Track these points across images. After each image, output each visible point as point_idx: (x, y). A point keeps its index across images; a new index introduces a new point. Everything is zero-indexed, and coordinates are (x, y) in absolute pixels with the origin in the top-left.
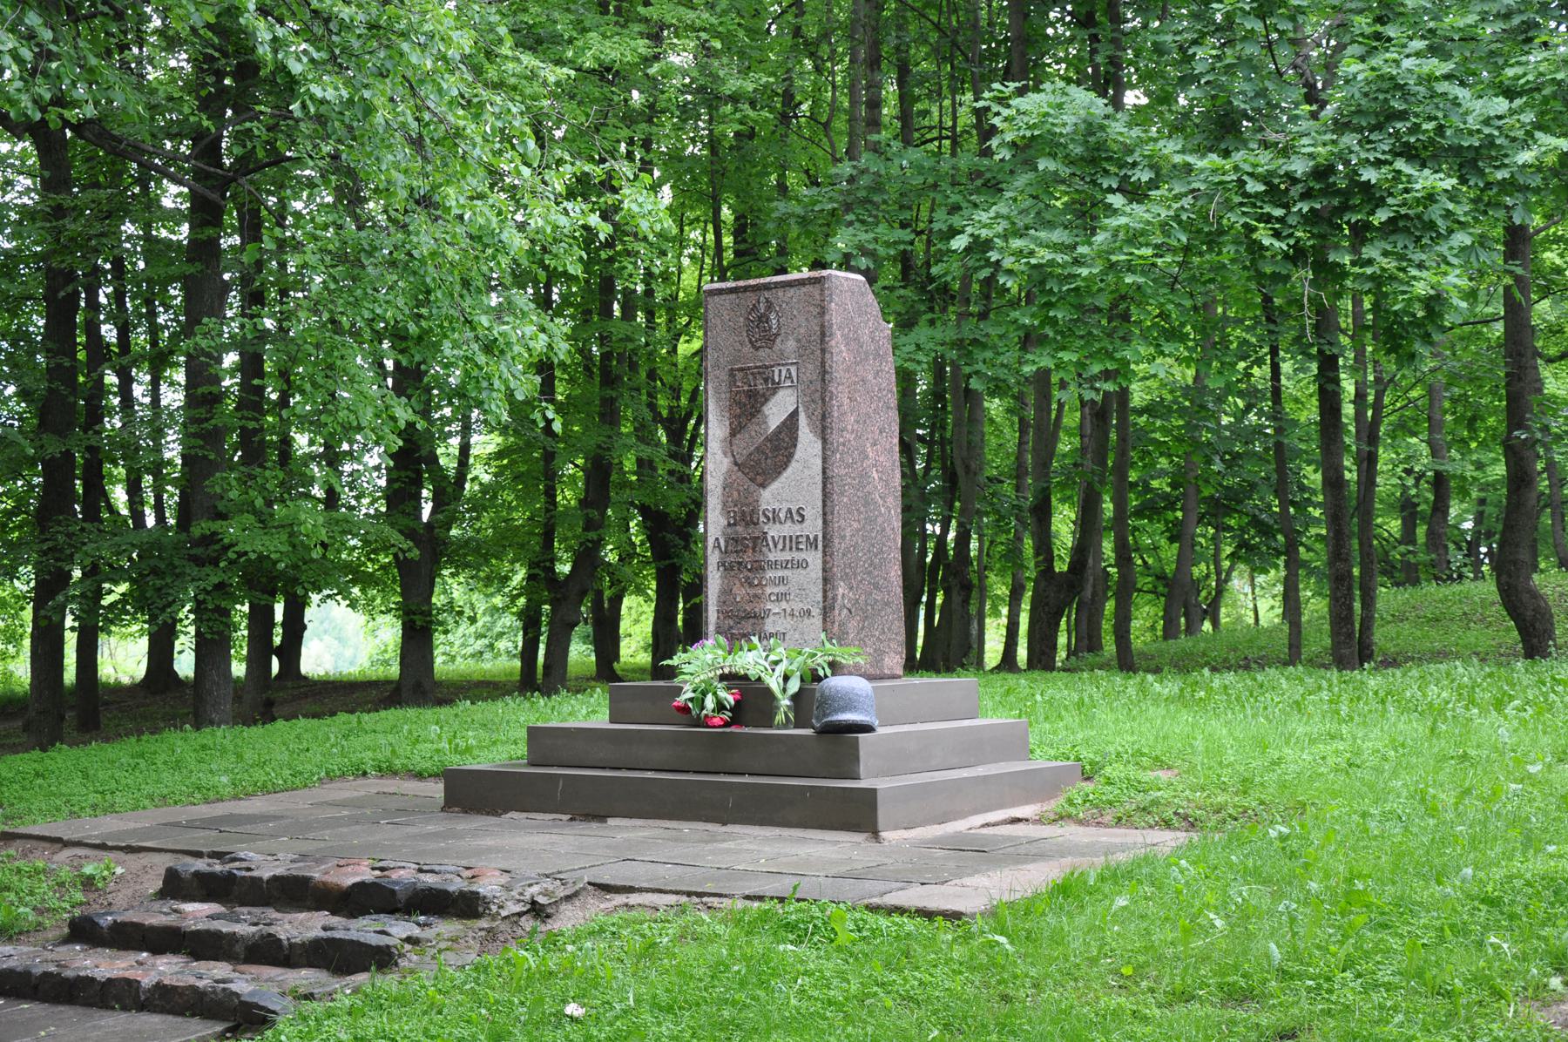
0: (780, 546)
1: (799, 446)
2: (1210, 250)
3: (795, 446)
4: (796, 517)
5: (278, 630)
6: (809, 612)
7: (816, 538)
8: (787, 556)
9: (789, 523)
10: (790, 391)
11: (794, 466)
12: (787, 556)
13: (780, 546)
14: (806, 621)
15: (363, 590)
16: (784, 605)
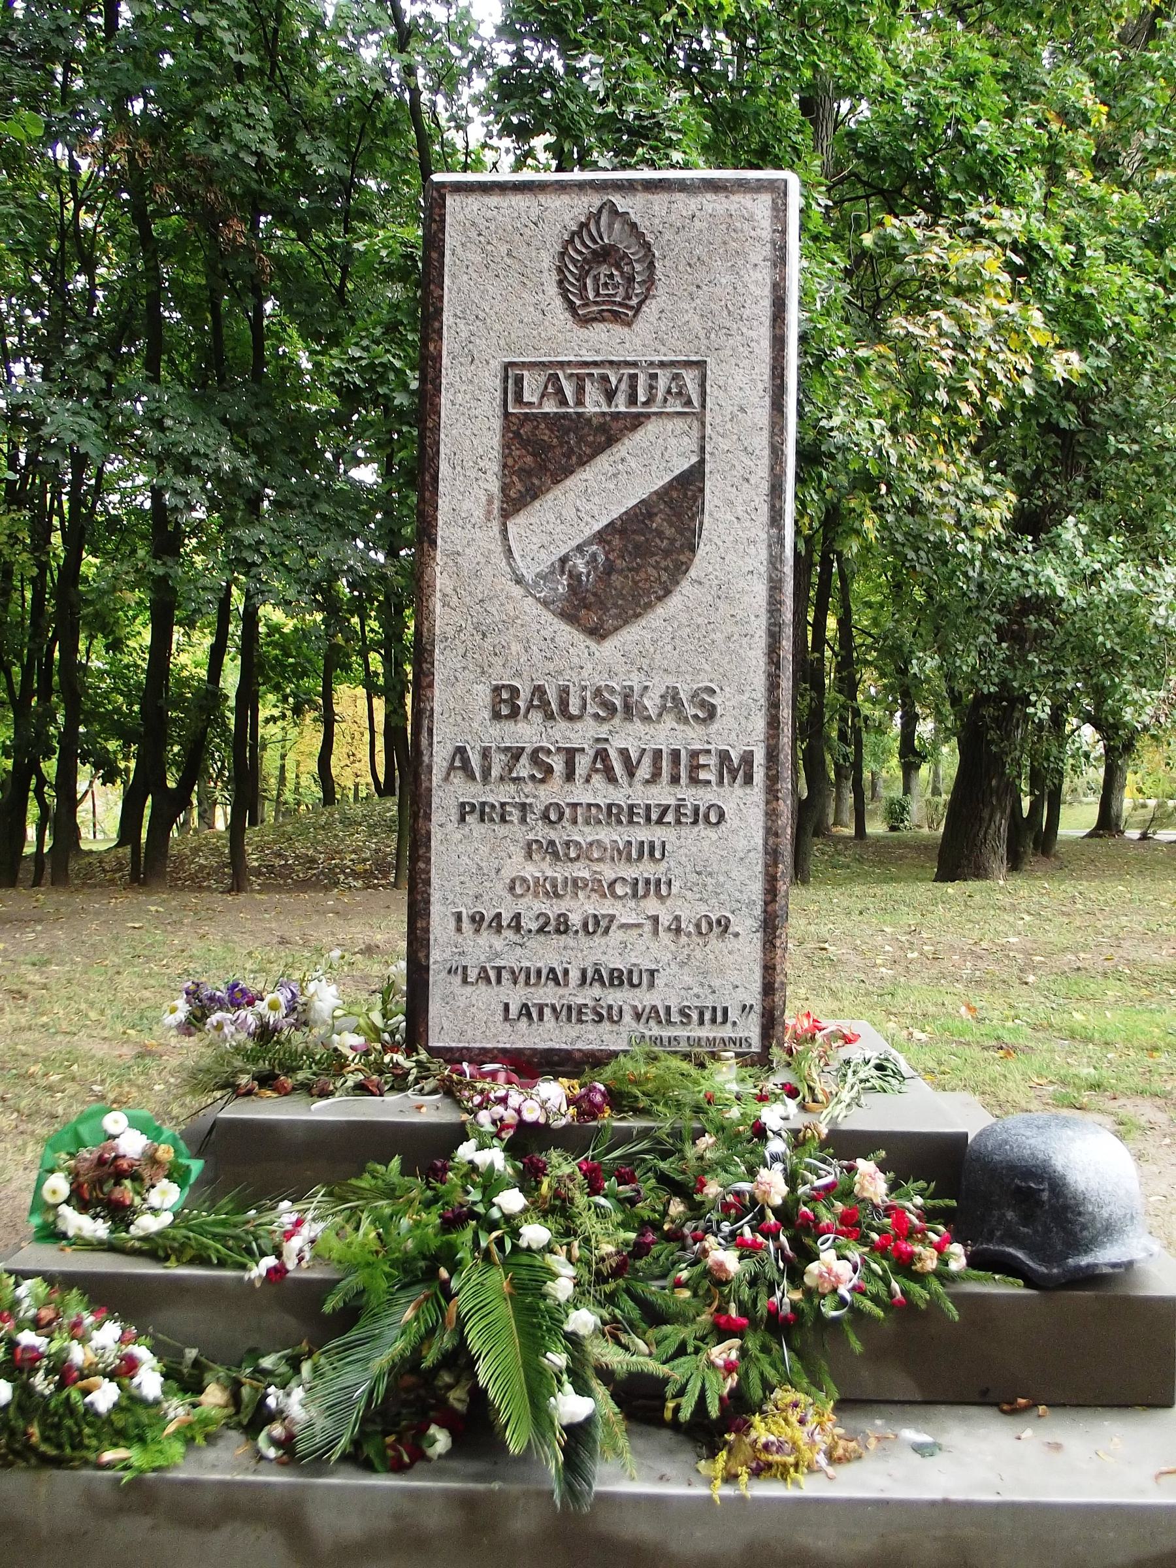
0: (644, 771)
1: (701, 552)
2: (965, 501)
3: (693, 549)
4: (691, 711)
5: (32, 787)
6: (724, 926)
7: (747, 759)
8: (663, 795)
9: (669, 721)
10: (680, 424)
11: (685, 594)
12: (663, 795)
13: (644, 771)
14: (714, 942)
15: (267, 364)
16: (652, 906)
